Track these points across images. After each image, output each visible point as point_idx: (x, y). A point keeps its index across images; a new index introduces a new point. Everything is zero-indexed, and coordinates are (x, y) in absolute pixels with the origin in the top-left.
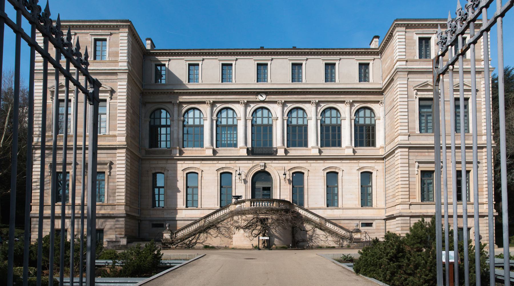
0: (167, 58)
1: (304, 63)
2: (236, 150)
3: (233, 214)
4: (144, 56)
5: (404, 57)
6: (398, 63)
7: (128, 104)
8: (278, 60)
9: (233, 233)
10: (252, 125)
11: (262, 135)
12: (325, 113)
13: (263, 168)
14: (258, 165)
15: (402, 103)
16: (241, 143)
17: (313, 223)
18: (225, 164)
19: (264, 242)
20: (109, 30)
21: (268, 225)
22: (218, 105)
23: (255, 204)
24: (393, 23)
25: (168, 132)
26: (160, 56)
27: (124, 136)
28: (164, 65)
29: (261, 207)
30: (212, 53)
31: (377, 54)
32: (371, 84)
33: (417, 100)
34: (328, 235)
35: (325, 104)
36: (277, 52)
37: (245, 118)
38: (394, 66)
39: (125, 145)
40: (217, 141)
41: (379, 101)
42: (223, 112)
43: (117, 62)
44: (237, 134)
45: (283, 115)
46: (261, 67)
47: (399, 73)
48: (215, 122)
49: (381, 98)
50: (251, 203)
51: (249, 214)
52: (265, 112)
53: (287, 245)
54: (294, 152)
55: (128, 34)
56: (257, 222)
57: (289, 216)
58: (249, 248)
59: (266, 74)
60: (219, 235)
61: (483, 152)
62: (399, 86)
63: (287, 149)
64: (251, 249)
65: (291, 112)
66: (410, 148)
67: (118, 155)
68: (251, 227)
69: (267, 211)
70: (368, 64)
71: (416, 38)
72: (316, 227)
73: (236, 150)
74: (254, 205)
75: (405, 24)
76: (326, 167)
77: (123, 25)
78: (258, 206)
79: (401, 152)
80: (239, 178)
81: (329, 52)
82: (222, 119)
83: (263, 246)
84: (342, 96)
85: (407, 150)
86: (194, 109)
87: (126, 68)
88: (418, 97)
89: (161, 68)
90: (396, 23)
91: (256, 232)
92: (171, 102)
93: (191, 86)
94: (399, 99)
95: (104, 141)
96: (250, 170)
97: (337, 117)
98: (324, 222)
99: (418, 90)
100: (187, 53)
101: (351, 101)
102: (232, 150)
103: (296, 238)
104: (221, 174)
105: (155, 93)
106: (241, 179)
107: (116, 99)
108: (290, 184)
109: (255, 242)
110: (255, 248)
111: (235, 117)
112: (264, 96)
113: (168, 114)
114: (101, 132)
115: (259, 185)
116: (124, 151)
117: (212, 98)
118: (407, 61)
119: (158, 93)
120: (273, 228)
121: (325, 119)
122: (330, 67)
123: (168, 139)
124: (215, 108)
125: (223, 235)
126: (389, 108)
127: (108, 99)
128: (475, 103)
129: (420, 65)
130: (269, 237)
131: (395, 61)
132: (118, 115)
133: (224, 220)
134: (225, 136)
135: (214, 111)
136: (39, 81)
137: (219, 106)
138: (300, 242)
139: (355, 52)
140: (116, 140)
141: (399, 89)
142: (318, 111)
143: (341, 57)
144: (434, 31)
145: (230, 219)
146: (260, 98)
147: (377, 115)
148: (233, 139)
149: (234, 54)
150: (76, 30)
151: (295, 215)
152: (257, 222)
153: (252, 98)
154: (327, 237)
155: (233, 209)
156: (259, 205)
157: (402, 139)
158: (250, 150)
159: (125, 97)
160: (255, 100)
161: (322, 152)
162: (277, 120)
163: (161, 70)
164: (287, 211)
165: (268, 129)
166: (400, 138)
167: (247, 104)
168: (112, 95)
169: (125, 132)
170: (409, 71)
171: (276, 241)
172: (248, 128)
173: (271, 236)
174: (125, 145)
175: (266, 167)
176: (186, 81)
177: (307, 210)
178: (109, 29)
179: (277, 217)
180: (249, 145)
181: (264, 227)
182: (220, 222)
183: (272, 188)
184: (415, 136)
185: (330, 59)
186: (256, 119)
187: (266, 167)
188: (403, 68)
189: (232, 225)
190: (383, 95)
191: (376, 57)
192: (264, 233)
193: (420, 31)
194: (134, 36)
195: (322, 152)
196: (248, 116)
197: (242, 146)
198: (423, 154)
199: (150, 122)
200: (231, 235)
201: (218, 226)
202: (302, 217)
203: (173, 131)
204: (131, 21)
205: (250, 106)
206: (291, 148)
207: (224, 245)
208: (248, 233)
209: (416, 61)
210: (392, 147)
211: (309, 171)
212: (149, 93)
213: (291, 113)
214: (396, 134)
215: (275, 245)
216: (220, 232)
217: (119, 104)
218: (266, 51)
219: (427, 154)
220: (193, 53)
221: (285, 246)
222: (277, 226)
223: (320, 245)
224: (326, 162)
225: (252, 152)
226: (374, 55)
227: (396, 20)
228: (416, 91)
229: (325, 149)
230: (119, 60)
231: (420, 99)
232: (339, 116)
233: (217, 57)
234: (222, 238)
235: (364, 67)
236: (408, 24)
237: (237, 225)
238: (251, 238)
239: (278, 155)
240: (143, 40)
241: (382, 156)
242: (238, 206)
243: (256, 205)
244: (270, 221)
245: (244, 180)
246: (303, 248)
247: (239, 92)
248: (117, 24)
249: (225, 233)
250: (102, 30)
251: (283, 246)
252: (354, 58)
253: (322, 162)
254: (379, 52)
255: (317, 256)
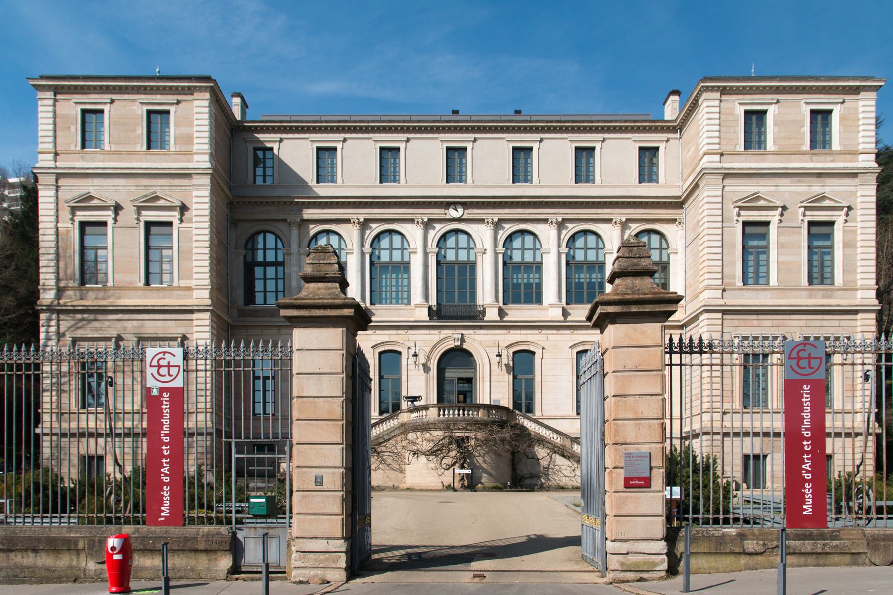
0: (278, 136)
1: (535, 146)
2: (408, 309)
3: (405, 429)
4: (231, 133)
5: (717, 147)
6: (706, 158)
7: (211, 231)
8: (486, 141)
9: (407, 462)
10: (438, 263)
11: (456, 293)
12: (574, 241)
13: (458, 343)
14: (449, 338)
15: (711, 231)
16: (417, 295)
17: (550, 446)
18: (387, 336)
19: (463, 479)
20: (173, 94)
21: (470, 449)
22: (374, 226)
23: (446, 412)
24: (698, 84)
25: (280, 275)
26: (264, 133)
27: (207, 289)
28: (272, 149)
29: (456, 418)
30: (361, 127)
31: (674, 130)
32: (662, 186)
33: (740, 225)
34: (576, 466)
35: (574, 225)
36: (485, 127)
37: (425, 250)
38: (700, 160)
39: (210, 306)
40: (371, 291)
41: (675, 220)
42: (384, 238)
43: (190, 153)
44: (409, 279)
45: (496, 246)
46: (455, 155)
47: (706, 177)
48: (367, 257)
49: (680, 214)
50: (439, 410)
51: (436, 429)
52: (463, 238)
53: (502, 484)
54: (518, 313)
55: (210, 103)
56: (450, 443)
57: (507, 433)
58: (437, 488)
59: (462, 165)
60: (380, 466)
61: (857, 320)
62: (706, 200)
63: (504, 307)
64: (440, 490)
65: (510, 238)
66: (724, 312)
67: (195, 323)
68: (439, 452)
69: (468, 424)
70: (657, 149)
71: (740, 111)
72: (555, 452)
73: (408, 309)
74: (444, 415)
75: (719, 87)
76: (576, 342)
77: (201, 87)
78: (451, 416)
79: (708, 319)
80: (415, 362)
81: (583, 126)
82: (382, 251)
83: (460, 485)
84: (606, 211)
85: (719, 315)
86: (328, 232)
87: (208, 165)
88: (741, 219)
89: (264, 155)
90: (702, 84)
91: (448, 461)
92: (285, 220)
93: (324, 190)
94: (706, 224)
95: (170, 298)
96: (434, 346)
97: (597, 249)
98: (570, 443)
99: (741, 208)
100: (314, 127)
101: (624, 220)
102: (401, 309)
103: (519, 472)
104: (380, 353)
105: (256, 203)
106: (417, 363)
107: (190, 221)
108: (508, 373)
109: (447, 479)
110: (447, 488)
111: (405, 247)
112: (461, 211)
113: (279, 241)
114: (164, 280)
115: (451, 374)
116: (207, 315)
117: (362, 214)
118: (722, 155)
119: (261, 203)
120: (480, 456)
121: (574, 253)
122: (584, 153)
123: (280, 288)
124: (368, 232)
125: (388, 465)
126: (692, 236)
127: (176, 222)
128: (849, 233)
129: (746, 161)
130: (472, 469)
131: (701, 153)
132: (195, 250)
133: (389, 439)
134: (389, 280)
135: (366, 237)
136: (47, 187)
137: (376, 228)
138: (526, 478)
139: (632, 127)
140: (192, 296)
141: (706, 206)
142: (562, 237)
143: (606, 135)
144: (772, 99)
145: (400, 437)
146: (453, 213)
147: (672, 245)
148: (402, 289)
149: (402, 130)
150: (113, 93)
151: (518, 432)
152: (450, 443)
153: (437, 213)
154: (574, 470)
155: (405, 420)
156: (454, 414)
157: (711, 297)
158: (435, 309)
159: (207, 219)
160: (442, 217)
161: (570, 314)
162: (484, 253)
163: (265, 158)
164: (502, 424)
165: (468, 270)
166: (707, 294)
167: (428, 225)
168: (182, 214)
169: (208, 282)
170: (725, 174)
171: (485, 479)
172: (430, 268)
173: (473, 466)
174: (210, 306)
175: (465, 342)
176: (312, 180)
177: (536, 421)
178: (173, 92)
179: (484, 435)
180: (433, 301)
181: (462, 453)
182: (382, 443)
183: (476, 380)
184: (735, 290)
185: (585, 139)
186: (445, 252)
187: (465, 342)
188: (714, 169)
189: (404, 448)
190: (683, 208)
191: (671, 135)
192: (463, 464)
193: (747, 98)
194: (219, 105)
195: (570, 314)
196: (429, 246)
197: (418, 303)
198: (749, 322)
199: (245, 257)
200: (403, 467)
201: (379, 450)
202: (530, 434)
203: (290, 274)
204: (215, 80)
205: (434, 228)
206: (510, 306)
207: (390, 484)
208: (434, 462)
209: (739, 154)
210: (695, 309)
211: (543, 348)
212: (244, 203)
213: (511, 241)
214: (701, 286)
215: (482, 484)
216: (383, 461)
217: (195, 231)
218: (463, 124)
219: (755, 322)
220: (326, 127)
221: (499, 485)
222: (487, 453)
223: (562, 484)
224: (575, 332)
225: (436, 314)
226: (668, 133)
227: (705, 79)
228: (737, 209)
229: (574, 309)
230: (195, 151)
231: (746, 224)
232: (601, 245)
233: (371, 135)
234: (387, 472)
235: (648, 155)
236: (725, 87)
237: (414, 448)
238: (441, 471)
239: (486, 319)
240: (228, 97)
241: (679, 321)
242: (415, 414)
243: (449, 414)
244: (472, 442)
245: (423, 364)
246: (531, 489)
247: (413, 203)
248: (191, 84)
249: (392, 463)
250: (161, 94)
251: (495, 484)
252: (629, 138)
253: (568, 332)
254: (677, 128)
255: (548, 499)
